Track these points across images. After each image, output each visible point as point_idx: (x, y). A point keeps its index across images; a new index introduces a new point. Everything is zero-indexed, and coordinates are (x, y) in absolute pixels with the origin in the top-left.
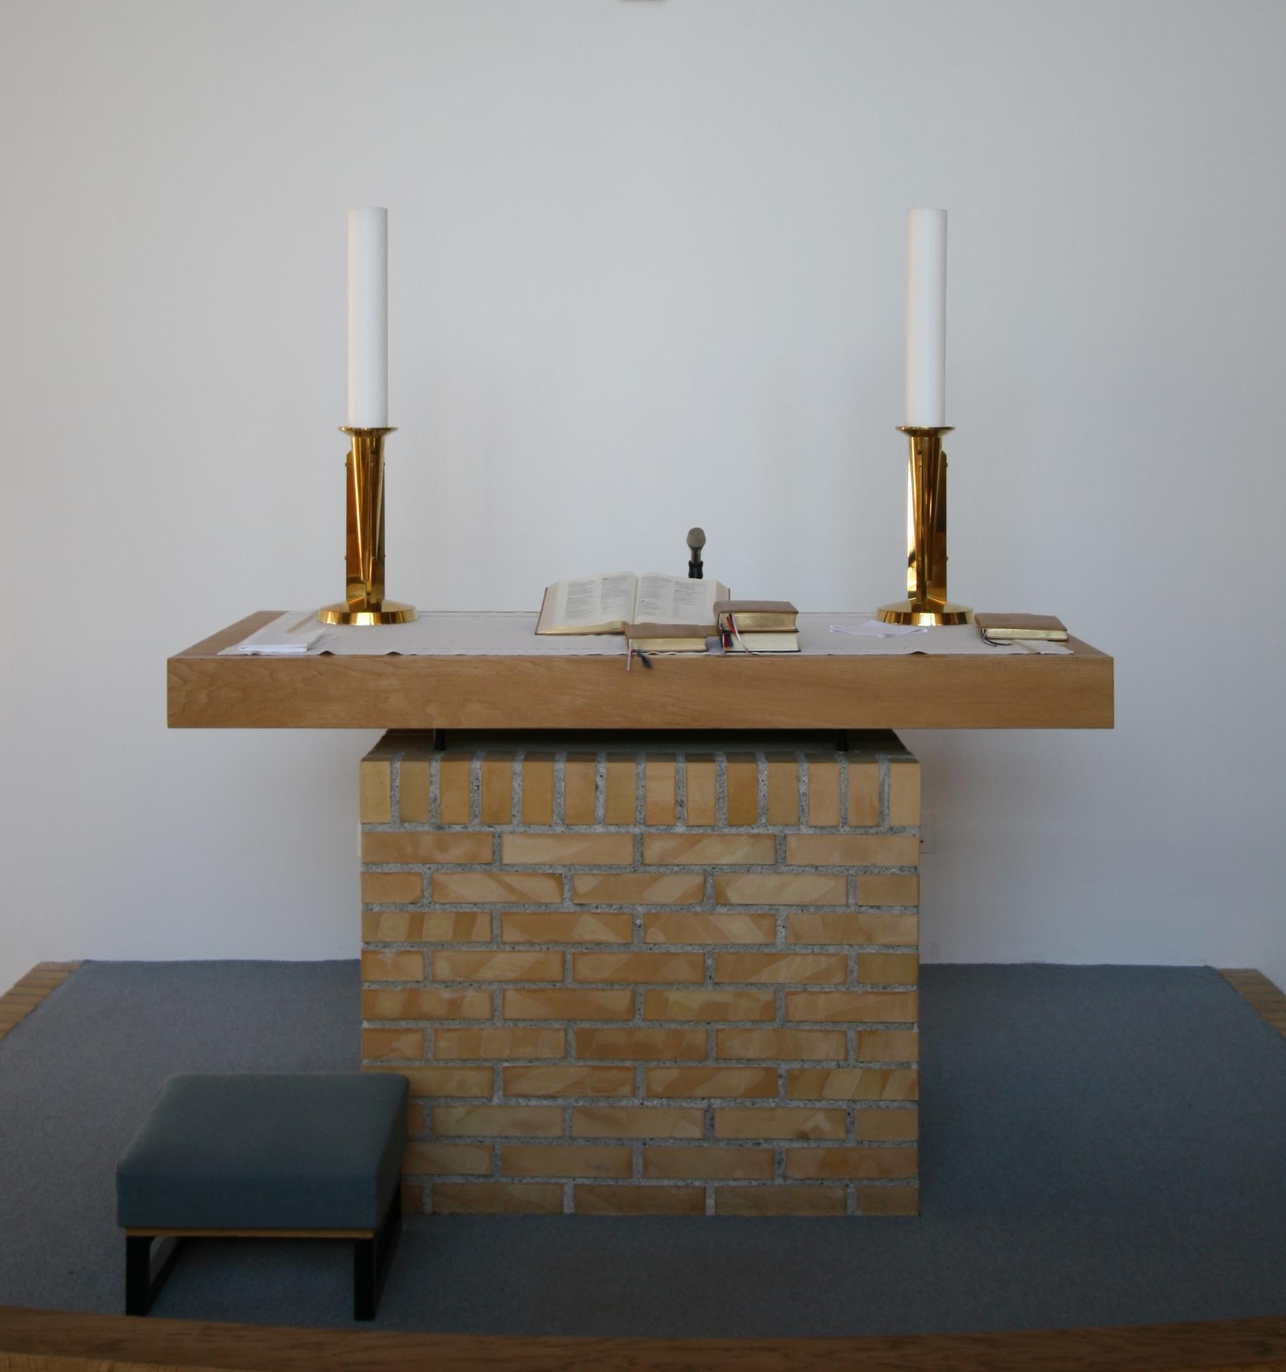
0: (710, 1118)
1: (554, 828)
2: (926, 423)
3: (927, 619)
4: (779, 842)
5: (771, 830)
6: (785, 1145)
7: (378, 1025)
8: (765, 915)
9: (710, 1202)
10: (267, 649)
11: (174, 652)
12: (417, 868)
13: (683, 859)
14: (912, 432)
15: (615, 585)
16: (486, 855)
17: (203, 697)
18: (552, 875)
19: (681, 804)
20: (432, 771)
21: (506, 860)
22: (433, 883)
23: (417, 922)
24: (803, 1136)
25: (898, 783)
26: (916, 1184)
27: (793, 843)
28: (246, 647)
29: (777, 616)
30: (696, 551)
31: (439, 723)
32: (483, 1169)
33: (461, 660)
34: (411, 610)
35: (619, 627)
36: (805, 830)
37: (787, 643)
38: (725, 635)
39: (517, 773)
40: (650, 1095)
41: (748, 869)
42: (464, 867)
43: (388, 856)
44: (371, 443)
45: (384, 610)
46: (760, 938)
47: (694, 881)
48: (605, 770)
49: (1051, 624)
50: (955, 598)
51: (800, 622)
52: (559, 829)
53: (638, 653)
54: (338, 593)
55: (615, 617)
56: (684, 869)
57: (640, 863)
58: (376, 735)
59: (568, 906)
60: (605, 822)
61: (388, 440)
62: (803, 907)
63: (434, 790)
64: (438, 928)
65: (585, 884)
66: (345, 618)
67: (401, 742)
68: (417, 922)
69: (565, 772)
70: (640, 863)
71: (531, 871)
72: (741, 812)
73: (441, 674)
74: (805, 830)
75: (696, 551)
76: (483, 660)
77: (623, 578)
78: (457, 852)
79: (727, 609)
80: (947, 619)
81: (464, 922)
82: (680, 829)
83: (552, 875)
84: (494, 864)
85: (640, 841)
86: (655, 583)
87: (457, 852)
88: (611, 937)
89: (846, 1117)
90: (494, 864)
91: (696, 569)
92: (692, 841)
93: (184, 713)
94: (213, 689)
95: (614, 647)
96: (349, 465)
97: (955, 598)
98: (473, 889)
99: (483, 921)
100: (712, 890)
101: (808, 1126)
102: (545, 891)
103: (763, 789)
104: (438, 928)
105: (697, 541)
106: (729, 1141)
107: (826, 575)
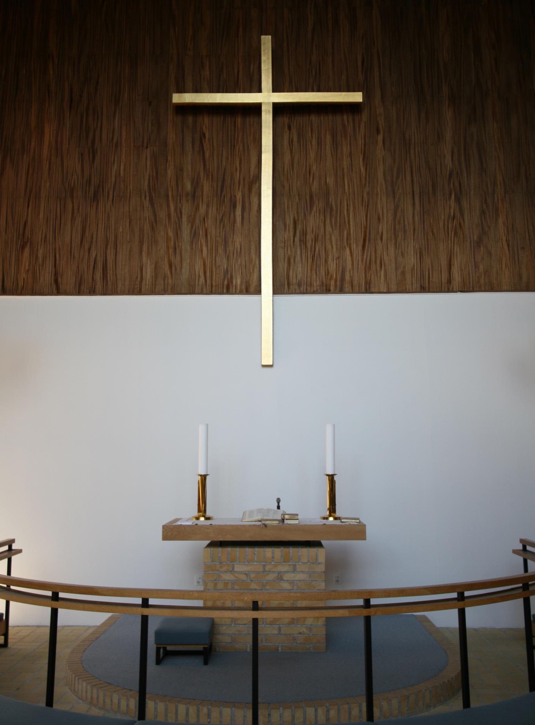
0: (280, 629)
1: (246, 562)
2: (330, 473)
3: (331, 519)
4: (295, 566)
5: (293, 563)
6: (296, 635)
7: (367, 184)
8: (292, 582)
9: (280, 649)
10: (183, 524)
11: (163, 524)
12: (216, 572)
13: (274, 570)
14: (327, 475)
15: (259, 511)
16: (231, 569)
17: (170, 534)
18: (245, 574)
19: (273, 557)
20: (219, 550)
21: (235, 570)
22: (219, 575)
23: (216, 585)
24: (300, 633)
25: (320, 554)
26: (325, 644)
27: (297, 566)
28: (179, 523)
29: (294, 516)
30: (278, 503)
31: (221, 539)
32: (230, 641)
33: (226, 526)
34: (213, 517)
35: (260, 519)
36: (300, 563)
37: (296, 522)
38: (283, 520)
39: (238, 551)
40: (267, 624)
41: (288, 572)
42: (226, 572)
43: (209, 570)
44: (204, 478)
45: (206, 516)
46: (290, 588)
47: (276, 575)
48: (257, 550)
49: (358, 519)
50: (338, 514)
51: (299, 517)
52: (247, 563)
53: (264, 524)
54: (196, 514)
55: (259, 518)
56: (274, 572)
57: (264, 571)
58: (208, 542)
59: (249, 581)
60: (257, 562)
61: (208, 477)
62: (300, 581)
63: (220, 555)
64: (220, 586)
65: (252, 576)
66: (198, 518)
67: (213, 544)
68: (216, 585)
69: (248, 550)
70: (264, 571)
71: (241, 573)
72: (286, 559)
73: (222, 529)
74: (300, 563)
75: (278, 503)
76: (231, 525)
77: (261, 509)
78: (224, 569)
79: (284, 515)
80: (336, 519)
81: (226, 584)
82: (273, 563)
83: (245, 574)
84: (232, 571)
85: (264, 566)
86: (269, 510)
87: (224, 569)
88: (258, 588)
89: (310, 629)
90: (232, 571)
91: (279, 507)
92: (276, 566)
93: (166, 537)
94: (172, 532)
95: (259, 523)
96: (199, 483)
97: (338, 514)
98: (228, 577)
99: (230, 584)
100: (280, 577)
101: (301, 631)
102: (243, 577)
103: (291, 554)
104: (220, 586)
105: (278, 501)
106: (284, 634)
107: (309, 509)
